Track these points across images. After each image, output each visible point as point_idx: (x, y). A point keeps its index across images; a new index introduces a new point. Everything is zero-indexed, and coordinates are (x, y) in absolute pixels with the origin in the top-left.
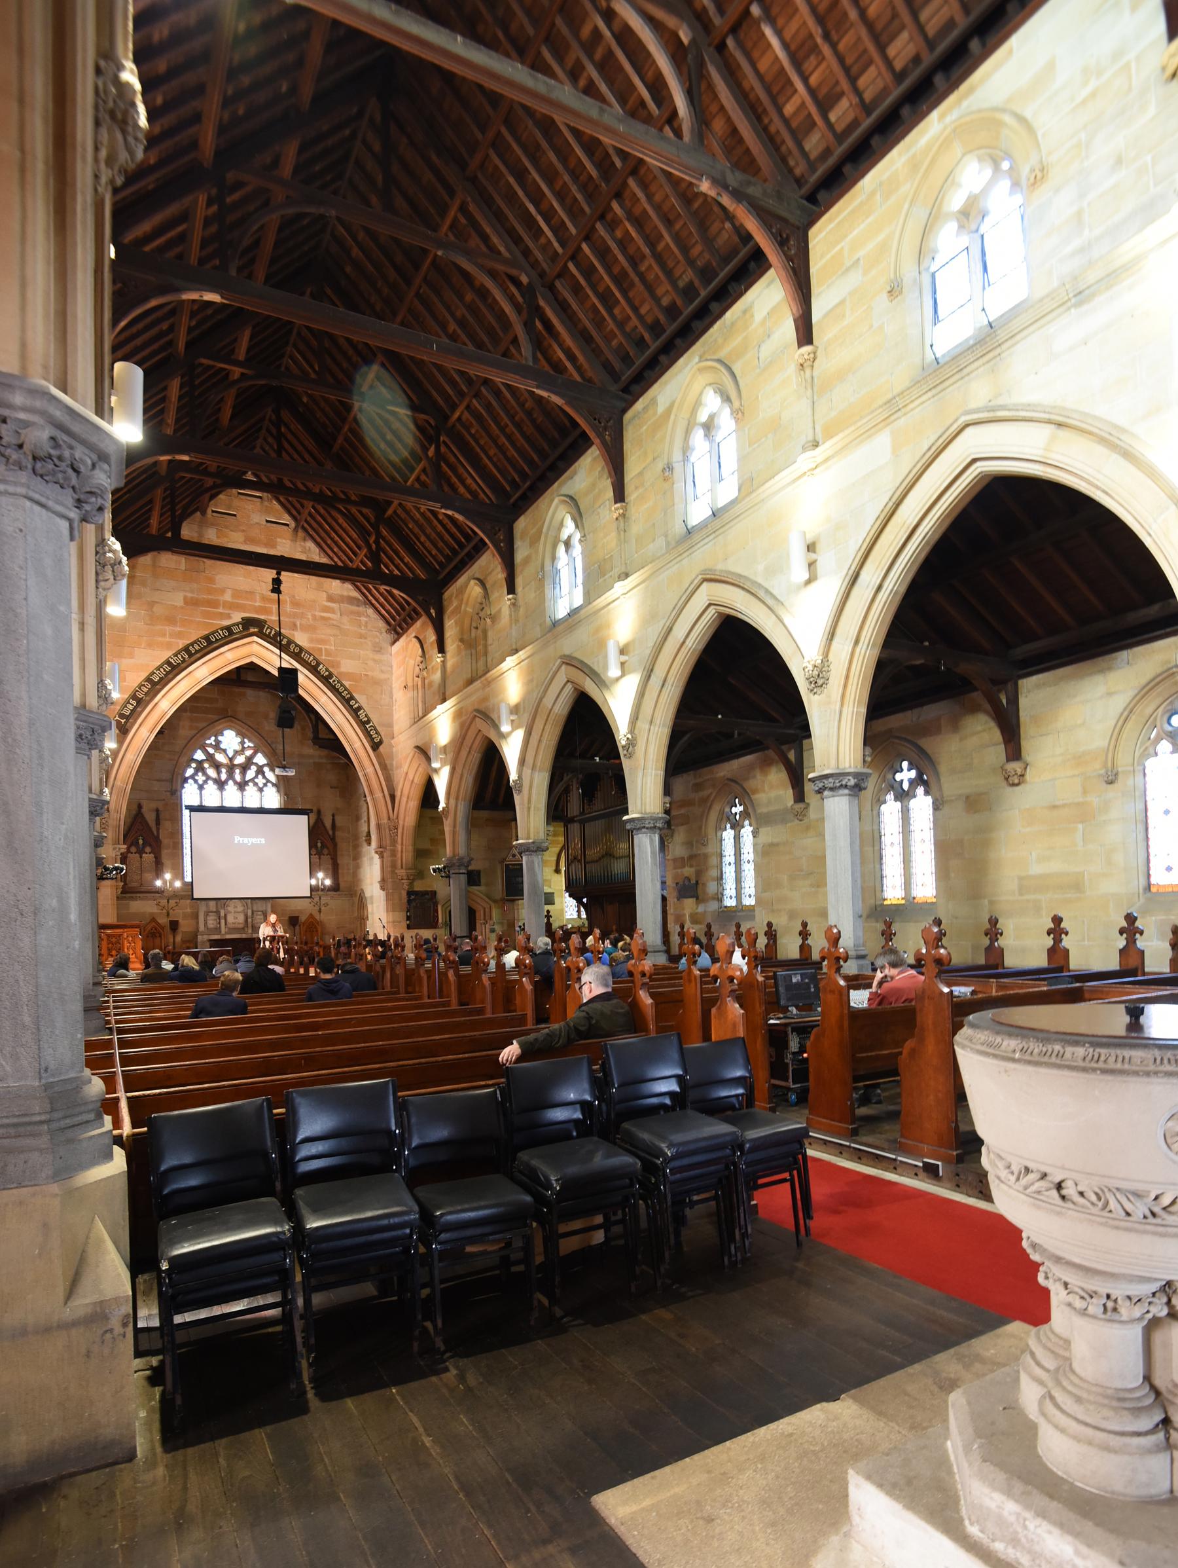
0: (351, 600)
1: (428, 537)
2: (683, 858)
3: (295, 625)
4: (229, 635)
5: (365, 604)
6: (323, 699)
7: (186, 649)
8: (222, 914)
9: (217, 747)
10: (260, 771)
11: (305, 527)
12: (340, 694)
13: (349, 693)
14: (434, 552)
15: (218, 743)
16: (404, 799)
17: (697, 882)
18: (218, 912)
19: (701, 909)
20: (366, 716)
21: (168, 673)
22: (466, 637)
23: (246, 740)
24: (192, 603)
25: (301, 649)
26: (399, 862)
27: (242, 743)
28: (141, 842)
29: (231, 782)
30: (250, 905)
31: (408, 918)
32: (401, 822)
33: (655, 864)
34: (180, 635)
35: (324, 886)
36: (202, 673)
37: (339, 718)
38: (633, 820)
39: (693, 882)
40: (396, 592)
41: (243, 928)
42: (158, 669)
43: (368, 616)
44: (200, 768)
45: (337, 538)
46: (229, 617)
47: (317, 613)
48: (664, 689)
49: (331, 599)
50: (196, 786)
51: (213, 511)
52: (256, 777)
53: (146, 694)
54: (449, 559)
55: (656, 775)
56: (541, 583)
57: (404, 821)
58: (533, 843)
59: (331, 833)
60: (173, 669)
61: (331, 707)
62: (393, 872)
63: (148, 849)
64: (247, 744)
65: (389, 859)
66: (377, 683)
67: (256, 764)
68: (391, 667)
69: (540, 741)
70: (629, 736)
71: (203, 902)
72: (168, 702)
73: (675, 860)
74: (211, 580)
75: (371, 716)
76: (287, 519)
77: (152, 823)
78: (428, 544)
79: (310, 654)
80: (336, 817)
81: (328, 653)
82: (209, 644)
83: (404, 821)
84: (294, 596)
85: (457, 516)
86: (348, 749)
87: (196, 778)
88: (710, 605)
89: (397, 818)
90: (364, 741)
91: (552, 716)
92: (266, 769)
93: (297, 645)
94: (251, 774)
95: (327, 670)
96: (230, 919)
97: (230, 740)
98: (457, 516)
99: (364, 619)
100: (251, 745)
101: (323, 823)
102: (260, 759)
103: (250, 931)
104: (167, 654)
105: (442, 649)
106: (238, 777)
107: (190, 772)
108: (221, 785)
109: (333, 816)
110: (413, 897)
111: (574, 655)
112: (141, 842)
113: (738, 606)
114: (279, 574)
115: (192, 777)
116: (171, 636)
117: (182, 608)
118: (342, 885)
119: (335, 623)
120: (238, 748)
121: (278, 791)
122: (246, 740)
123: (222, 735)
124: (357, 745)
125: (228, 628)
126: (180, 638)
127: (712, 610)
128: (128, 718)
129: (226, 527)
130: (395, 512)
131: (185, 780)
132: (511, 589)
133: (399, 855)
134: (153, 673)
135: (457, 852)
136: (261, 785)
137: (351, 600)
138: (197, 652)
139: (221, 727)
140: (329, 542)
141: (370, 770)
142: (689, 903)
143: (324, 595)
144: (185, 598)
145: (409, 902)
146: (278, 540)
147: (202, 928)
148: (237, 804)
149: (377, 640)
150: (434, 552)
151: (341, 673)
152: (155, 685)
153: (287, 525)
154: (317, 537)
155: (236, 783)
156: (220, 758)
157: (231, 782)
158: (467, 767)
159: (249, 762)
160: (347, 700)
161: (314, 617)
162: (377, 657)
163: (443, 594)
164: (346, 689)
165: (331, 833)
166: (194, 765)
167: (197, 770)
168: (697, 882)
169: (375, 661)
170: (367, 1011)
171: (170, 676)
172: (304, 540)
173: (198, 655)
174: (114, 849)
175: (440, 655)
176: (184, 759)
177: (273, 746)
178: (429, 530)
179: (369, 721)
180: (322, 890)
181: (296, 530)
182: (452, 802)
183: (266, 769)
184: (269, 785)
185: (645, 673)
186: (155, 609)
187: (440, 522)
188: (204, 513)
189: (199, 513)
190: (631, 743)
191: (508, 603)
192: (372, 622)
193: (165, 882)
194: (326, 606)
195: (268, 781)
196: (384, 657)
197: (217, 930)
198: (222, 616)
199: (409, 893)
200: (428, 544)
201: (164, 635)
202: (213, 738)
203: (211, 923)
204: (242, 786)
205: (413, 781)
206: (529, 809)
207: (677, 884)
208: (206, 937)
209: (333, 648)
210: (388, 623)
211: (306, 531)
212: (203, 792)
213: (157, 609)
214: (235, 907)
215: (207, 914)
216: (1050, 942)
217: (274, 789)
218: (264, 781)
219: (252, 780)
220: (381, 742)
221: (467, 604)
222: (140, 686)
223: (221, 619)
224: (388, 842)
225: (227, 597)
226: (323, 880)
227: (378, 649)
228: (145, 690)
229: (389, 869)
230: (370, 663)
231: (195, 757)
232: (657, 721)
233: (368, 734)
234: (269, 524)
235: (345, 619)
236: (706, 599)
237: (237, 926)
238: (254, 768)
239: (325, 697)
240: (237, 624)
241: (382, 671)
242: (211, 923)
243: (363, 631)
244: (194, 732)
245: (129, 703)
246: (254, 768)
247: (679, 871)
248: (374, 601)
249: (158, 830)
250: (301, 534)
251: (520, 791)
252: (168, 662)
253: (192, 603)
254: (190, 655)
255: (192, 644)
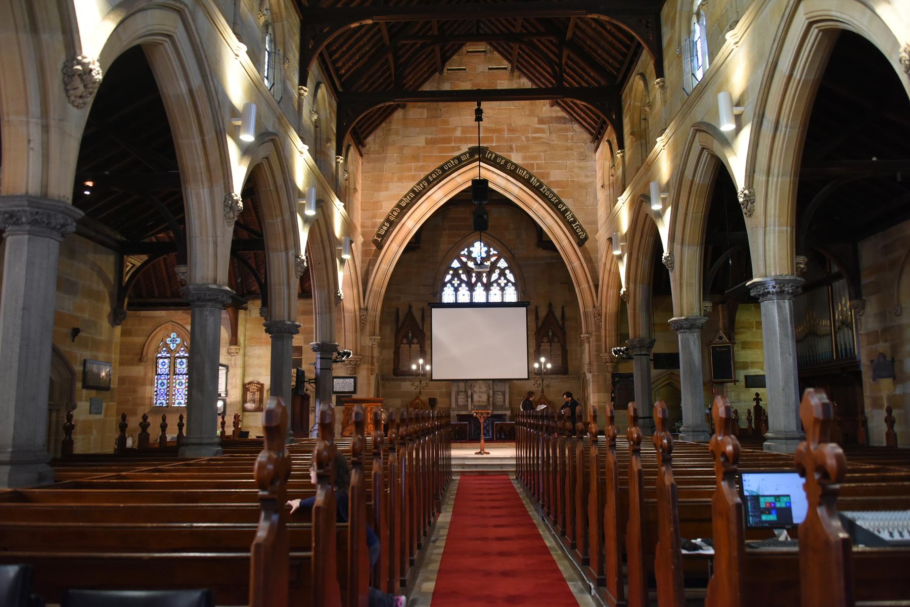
0: (559, 120)
1: (603, 48)
2: (876, 332)
3: (511, 148)
4: (459, 163)
5: (571, 121)
6: (535, 206)
7: (426, 179)
8: (469, 394)
9: (469, 257)
10: (502, 274)
11: (519, 67)
12: (549, 200)
13: (558, 198)
14: (610, 61)
15: (470, 252)
16: (605, 288)
17: (893, 360)
18: (466, 392)
19: (899, 391)
20: (573, 216)
21: (412, 199)
22: (636, 130)
23: (492, 249)
24: (431, 142)
25: (516, 166)
26: (603, 346)
27: (488, 252)
28: (410, 335)
29: (479, 284)
30: (491, 386)
31: (613, 399)
32: (604, 309)
33: (786, 335)
34: (422, 168)
35: (547, 369)
36: (439, 196)
37: (549, 221)
38: (755, 285)
39: (889, 359)
40: (578, 102)
41: (486, 406)
42: (405, 197)
43: (574, 131)
44: (456, 274)
45: (541, 70)
46: (459, 148)
47: (530, 135)
48: (778, 133)
49: (541, 121)
50: (453, 289)
51: (448, 70)
52: (499, 278)
53: (397, 217)
54: (621, 63)
55: (780, 232)
56: (679, 57)
57: (606, 308)
58: (686, 319)
59: (560, 323)
60: (416, 195)
61: (542, 212)
62: (598, 356)
63: (415, 341)
64: (493, 252)
65: (594, 344)
66: (582, 187)
67: (499, 268)
68: (595, 171)
69: (686, 214)
70: (746, 192)
71: (455, 384)
72: (412, 222)
73: (868, 334)
74: (446, 122)
75: (577, 216)
76: (505, 64)
77: (419, 320)
78: (604, 55)
79: (524, 170)
80: (565, 309)
81: (539, 167)
82: (443, 172)
83: (606, 308)
84: (510, 125)
85: (603, 18)
86: (558, 247)
87: (453, 282)
88: (810, 25)
89: (601, 306)
90: (571, 238)
91: (694, 188)
92: (507, 272)
93: (513, 164)
94: (495, 276)
95: (538, 181)
96: (476, 397)
97: (478, 249)
98: (603, 18)
99: (570, 134)
100: (495, 252)
101: (554, 316)
102: (502, 264)
103: (491, 408)
104: (411, 185)
105: (621, 146)
106: (485, 280)
107: (448, 277)
108: (471, 287)
109: (563, 308)
110: (617, 379)
111: (705, 120)
112: (410, 335)
113: (834, 13)
114: (479, 104)
115: (450, 282)
116: (416, 170)
117: (424, 147)
118: (571, 369)
119: (545, 140)
120: (484, 255)
121: (516, 289)
122: (492, 249)
123: (473, 246)
124: (565, 242)
125: (458, 158)
126: (422, 171)
127: (814, 32)
128: (382, 236)
129: (458, 80)
130: (574, 34)
131: (445, 285)
132: (660, 73)
133: (603, 339)
134: (402, 200)
135: (637, 333)
136: (503, 285)
137: (559, 120)
138: (434, 180)
139: (471, 240)
140: (537, 75)
141: (576, 264)
142: (886, 383)
143: (536, 119)
144: (426, 139)
145: (614, 383)
146: (498, 82)
147: (453, 405)
148: (483, 300)
149: (582, 150)
150: (610, 61)
151: (550, 182)
152: (403, 209)
153: (505, 69)
154: (527, 73)
155: (483, 284)
156: (471, 264)
157: (479, 284)
158: (642, 250)
159: (494, 266)
160: (556, 206)
161: (528, 139)
162: (582, 164)
163: (621, 96)
164: (555, 195)
165: (560, 323)
166: (451, 272)
167: (453, 276)
168: (893, 360)
169: (580, 168)
170: (181, 477)
171: (414, 201)
172: (519, 77)
173: (435, 182)
174: (371, 339)
175: (619, 151)
176: (443, 268)
177: (513, 252)
178: (602, 43)
179: (575, 221)
180: (545, 374)
181: (512, 71)
182: (632, 286)
183: (507, 272)
184: (510, 284)
185: (756, 120)
186: (404, 151)
187: (608, 31)
188: (441, 72)
189: (437, 73)
190: (750, 199)
191: (657, 86)
192: (578, 134)
193: (418, 366)
194: (537, 128)
195: (509, 281)
196: (589, 164)
197: (465, 407)
198: (454, 149)
199: (614, 375)
200: (604, 55)
201: (410, 170)
202: (466, 249)
203: (461, 401)
204: (487, 287)
205: (610, 270)
206: (681, 285)
207: (872, 361)
208: (456, 412)
209: (543, 162)
210: (591, 133)
211: (519, 70)
212: (474, 293)
213: (406, 151)
214: (480, 388)
215: (458, 393)
216: (755, 404)
217: (513, 288)
218: (505, 281)
219: (496, 281)
220: (586, 238)
221: (635, 99)
222: (393, 211)
223: (453, 151)
224: (594, 329)
225: (458, 133)
226: (545, 364)
227: (583, 158)
228: (396, 214)
229: (595, 353)
230: (576, 170)
231: (452, 266)
232: (775, 170)
233: (574, 232)
234: (491, 71)
235: (554, 136)
236: (804, 18)
237: (481, 404)
238: (497, 271)
239: (537, 204)
240: (465, 154)
241: (587, 176)
242: (461, 401)
243: (569, 144)
244: (451, 246)
245: (384, 225)
246: (497, 271)
247: (874, 346)
248: (578, 118)
249: (423, 325)
250: (516, 73)
251: (673, 268)
252: (413, 191)
253: (431, 142)
254: (429, 183)
255: (430, 174)
